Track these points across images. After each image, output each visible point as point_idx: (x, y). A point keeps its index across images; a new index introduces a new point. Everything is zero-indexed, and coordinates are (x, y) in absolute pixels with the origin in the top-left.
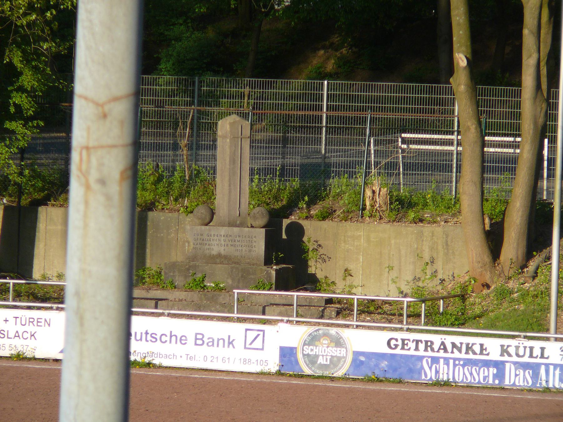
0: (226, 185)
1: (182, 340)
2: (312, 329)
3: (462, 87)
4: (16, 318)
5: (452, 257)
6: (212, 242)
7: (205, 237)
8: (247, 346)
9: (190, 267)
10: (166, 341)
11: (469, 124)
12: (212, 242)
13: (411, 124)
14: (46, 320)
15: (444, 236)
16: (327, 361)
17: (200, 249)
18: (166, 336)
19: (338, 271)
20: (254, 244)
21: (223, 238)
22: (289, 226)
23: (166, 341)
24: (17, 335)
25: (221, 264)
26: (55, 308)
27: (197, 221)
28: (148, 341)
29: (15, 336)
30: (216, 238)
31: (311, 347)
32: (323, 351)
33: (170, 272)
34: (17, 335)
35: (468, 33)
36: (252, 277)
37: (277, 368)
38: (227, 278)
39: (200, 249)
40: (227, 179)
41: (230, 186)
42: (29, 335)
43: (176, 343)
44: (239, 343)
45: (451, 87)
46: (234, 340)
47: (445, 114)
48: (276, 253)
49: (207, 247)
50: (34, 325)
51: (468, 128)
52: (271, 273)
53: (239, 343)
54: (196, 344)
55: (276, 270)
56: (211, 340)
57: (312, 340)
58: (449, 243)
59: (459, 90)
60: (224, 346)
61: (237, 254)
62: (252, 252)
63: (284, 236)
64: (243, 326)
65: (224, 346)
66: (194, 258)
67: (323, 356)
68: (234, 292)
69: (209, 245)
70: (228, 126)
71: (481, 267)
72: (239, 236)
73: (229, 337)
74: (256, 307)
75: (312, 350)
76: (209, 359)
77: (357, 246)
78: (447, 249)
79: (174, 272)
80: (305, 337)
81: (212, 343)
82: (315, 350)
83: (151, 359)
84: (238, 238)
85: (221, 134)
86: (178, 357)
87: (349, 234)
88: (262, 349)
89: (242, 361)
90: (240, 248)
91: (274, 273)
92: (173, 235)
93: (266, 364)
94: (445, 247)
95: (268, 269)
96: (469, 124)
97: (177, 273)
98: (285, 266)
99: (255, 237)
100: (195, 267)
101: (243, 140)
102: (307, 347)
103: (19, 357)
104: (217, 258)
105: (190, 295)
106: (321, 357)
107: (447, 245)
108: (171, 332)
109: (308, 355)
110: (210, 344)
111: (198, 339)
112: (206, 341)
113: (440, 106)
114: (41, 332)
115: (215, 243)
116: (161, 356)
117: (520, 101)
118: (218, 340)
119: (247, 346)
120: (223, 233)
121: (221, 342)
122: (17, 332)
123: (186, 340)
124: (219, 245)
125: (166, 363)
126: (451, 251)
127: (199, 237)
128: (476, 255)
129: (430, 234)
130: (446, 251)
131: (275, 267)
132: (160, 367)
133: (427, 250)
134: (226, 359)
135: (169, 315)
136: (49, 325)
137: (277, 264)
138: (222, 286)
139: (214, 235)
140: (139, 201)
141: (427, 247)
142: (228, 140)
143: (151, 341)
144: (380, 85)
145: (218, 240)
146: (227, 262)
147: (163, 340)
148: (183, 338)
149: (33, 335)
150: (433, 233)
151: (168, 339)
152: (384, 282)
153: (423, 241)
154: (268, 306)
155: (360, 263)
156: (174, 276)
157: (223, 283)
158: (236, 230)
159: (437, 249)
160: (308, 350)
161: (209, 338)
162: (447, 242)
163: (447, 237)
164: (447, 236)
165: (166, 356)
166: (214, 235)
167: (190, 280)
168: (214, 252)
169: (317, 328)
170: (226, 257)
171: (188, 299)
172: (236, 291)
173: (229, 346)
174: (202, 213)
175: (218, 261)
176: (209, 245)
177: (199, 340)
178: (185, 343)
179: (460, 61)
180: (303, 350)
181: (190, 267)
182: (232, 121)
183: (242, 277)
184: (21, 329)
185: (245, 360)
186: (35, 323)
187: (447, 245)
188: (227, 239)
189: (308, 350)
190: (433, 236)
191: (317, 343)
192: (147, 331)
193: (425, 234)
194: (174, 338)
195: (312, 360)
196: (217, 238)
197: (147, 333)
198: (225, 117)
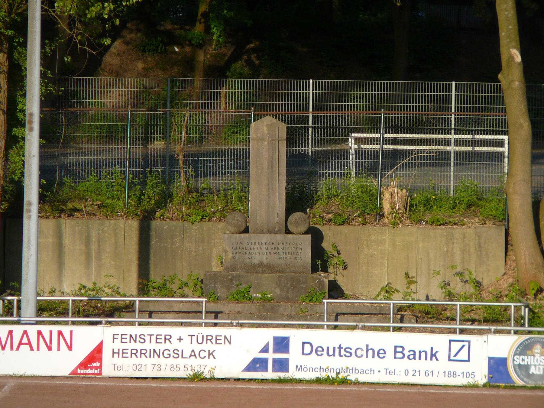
1: (381, 354)
2: (524, 337)
3: (517, 83)
4: (192, 336)
6: (253, 250)
7: (245, 245)
8: (452, 358)
10: (362, 356)
11: (522, 121)
12: (253, 250)
13: (404, 123)
14: (131, 336)
15: (477, 238)
16: (539, 371)
18: (205, 351)
19: (361, 278)
20: (300, 251)
21: (264, 246)
23: (362, 356)
24: (193, 354)
26: (235, 324)
27: (232, 229)
28: (342, 356)
29: (191, 356)
30: (257, 246)
31: (523, 357)
32: (535, 361)
33: (211, 284)
34: (193, 354)
35: (516, 27)
36: (303, 286)
37: (485, 380)
42: (207, 354)
43: (373, 357)
44: (443, 355)
45: (500, 85)
46: (437, 352)
47: (440, 111)
49: (247, 255)
50: (212, 343)
51: (521, 126)
53: (443, 355)
54: (395, 358)
56: (412, 353)
57: (524, 349)
58: (482, 245)
59: (513, 86)
60: (426, 359)
62: (297, 260)
64: (446, 338)
65: (426, 359)
66: (233, 268)
67: (535, 366)
68: (324, 302)
69: (249, 253)
70: (265, 128)
71: (535, 269)
72: (283, 244)
73: (432, 349)
75: (523, 360)
76: (411, 373)
77: (381, 250)
78: (481, 251)
79: (215, 283)
81: (414, 355)
82: (526, 360)
83: (346, 374)
84: (281, 246)
85: (254, 136)
86: (376, 372)
87: (373, 238)
88: (468, 361)
89: (447, 374)
90: (285, 256)
92: (178, 244)
93: (473, 376)
96: (522, 121)
97: (218, 285)
99: (301, 244)
100: (239, 277)
102: (518, 357)
103: (197, 377)
104: (259, 267)
106: (533, 367)
107: (480, 247)
108: (367, 346)
109: (519, 365)
110: (412, 357)
112: (406, 353)
113: (434, 104)
114: (220, 350)
115: (256, 251)
116: (357, 371)
117: (503, 96)
118: (420, 352)
119: (452, 358)
120: (264, 241)
121: (423, 355)
122: (193, 351)
123: (385, 353)
125: (362, 378)
126: (484, 253)
127: (238, 246)
128: (529, 256)
129: (462, 236)
130: (479, 253)
132: (357, 383)
133: (458, 253)
134: (429, 373)
135: (364, 328)
136: (230, 343)
138: (269, 296)
139: (255, 243)
141: (458, 249)
142: (266, 143)
143: (345, 355)
144: (434, 83)
145: (259, 248)
146: (270, 271)
147: (202, 356)
148: (382, 352)
149: (212, 354)
151: (364, 353)
153: (453, 243)
156: (215, 287)
160: (519, 360)
161: (409, 351)
164: (480, 238)
165: (363, 372)
166: (255, 243)
168: (256, 261)
169: (528, 336)
173: (431, 359)
174: (238, 220)
175: (260, 270)
176: (249, 253)
177: (399, 352)
178: (384, 357)
179: (515, 57)
180: (514, 360)
181: (233, 277)
182: (269, 123)
183: (291, 286)
184: (197, 348)
185: (450, 373)
186: (214, 341)
187: (480, 247)
188: (269, 247)
189: (519, 360)
191: (529, 352)
192: (340, 345)
193: (456, 236)
194: (370, 352)
195: (524, 369)
196: (259, 246)
197: (340, 347)
198: (258, 119)
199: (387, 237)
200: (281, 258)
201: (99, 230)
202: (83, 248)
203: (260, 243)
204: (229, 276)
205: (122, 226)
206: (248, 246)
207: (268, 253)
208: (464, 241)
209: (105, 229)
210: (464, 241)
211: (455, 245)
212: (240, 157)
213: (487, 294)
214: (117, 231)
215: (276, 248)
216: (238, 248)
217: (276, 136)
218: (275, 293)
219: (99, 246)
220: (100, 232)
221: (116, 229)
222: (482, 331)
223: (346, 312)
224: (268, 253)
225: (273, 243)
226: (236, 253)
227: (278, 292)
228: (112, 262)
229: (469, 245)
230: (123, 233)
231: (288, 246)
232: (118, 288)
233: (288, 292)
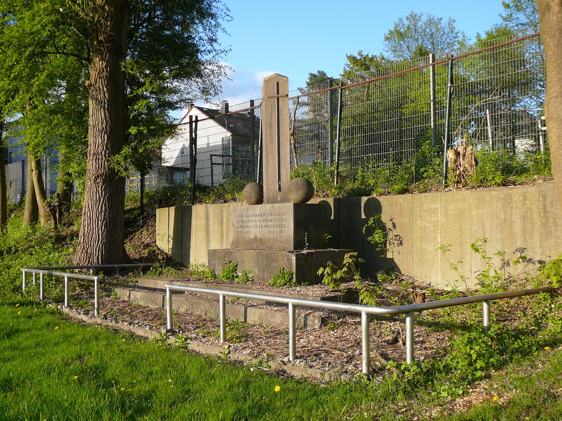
5: (553, 229)
7: (245, 218)
15: (541, 199)
19: (415, 255)
36: (275, 264)
38: (254, 267)
49: (246, 229)
61: (270, 236)
62: (283, 234)
77: (434, 222)
84: (270, 218)
87: (425, 207)
90: (272, 229)
94: (542, 215)
98: (332, 249)
101: (280, 99)
107: (545, 211)
120: (258, 213)
126: (551, 220)
129: (522, 198)
130: (544, 220)
140: (147, 190)
141: (518, 217)
150: (525, 196)
152: (467, 268)
153: (512, 208)
155: (437, 244)
156: (214, 264)
159: (531, 217)
162: (545, 206)
163: (544, 201)
164: (545, 198)
168: (252, 236)
183: (266, 265)
187: (545, 211)
190: (525, 200)
199: (439, 205)
200: (270, 232)
202: (220, 228)
206: (246, 219)
208: (524, 205)
210: (524, 205)
211: (514, 211)
213: (516, 343)
222: (37, 277)
223: (445, 303)
227: (256, 270)
229: (531, 209)
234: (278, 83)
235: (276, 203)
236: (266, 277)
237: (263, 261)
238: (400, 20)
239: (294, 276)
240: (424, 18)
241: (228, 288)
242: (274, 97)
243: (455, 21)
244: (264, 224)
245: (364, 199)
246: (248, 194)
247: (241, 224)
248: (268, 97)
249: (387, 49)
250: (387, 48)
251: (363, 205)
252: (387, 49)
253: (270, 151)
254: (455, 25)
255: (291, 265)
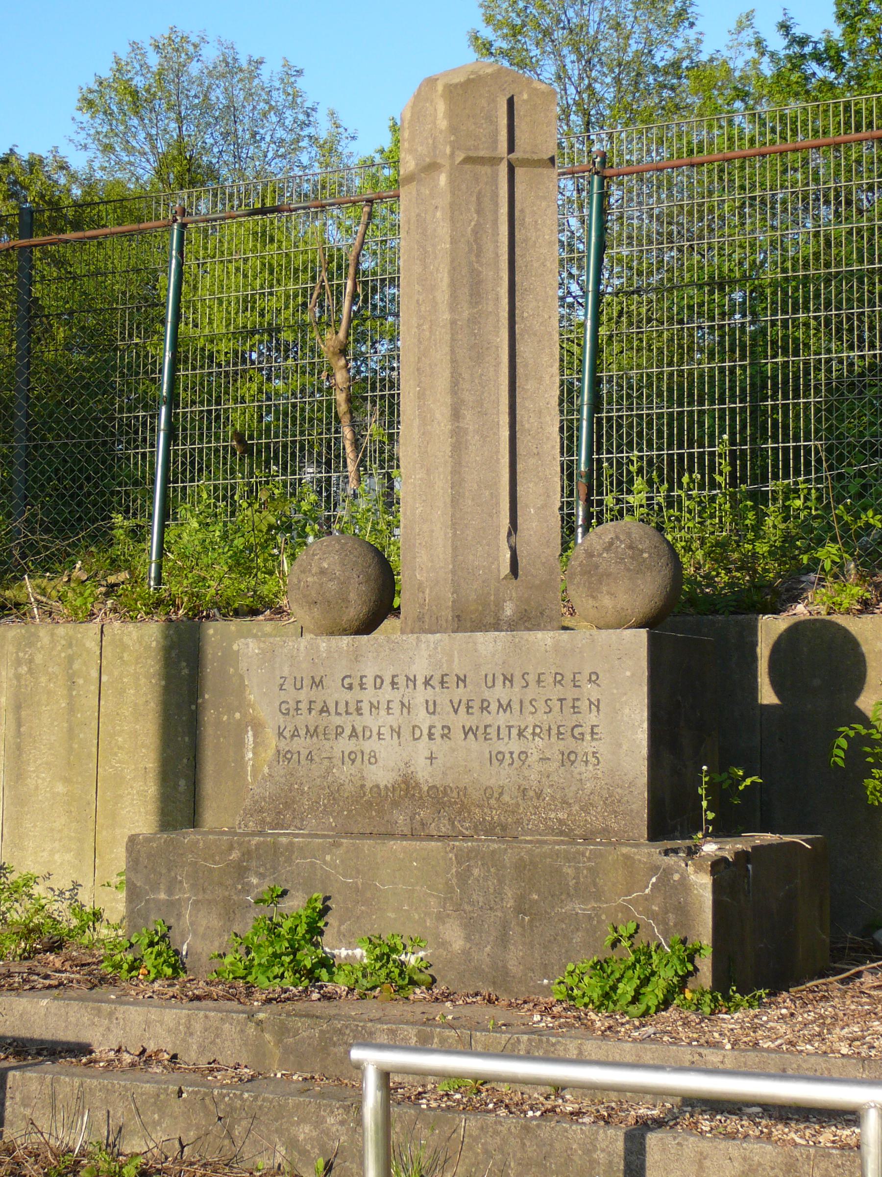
0: (441, 412)
6: (368, 720)
7: (334, 694)
9: (247, 854)
12: (368, 720)
17: (310, 758)
20: (592, 718)
22: (785, 645)
25: (413, 836)
30: (387, 693)
33: (155, 888)
36: (578, 907)
38: (441, 918)
39: (310, 758)
40: (443, 381)
41: (456, 415)
48: (722, 766)
49: (345, 745)
52: (684, 885)
55: (718, 866)
61: (501, 777)
63: (767, 696)
68: (359, 1067)
70: (441, 107)
72: (508, 679)
74: (577, 1132)
80: (702, 47)
84: (500, 692)
90: (515, 746)
91: (702, 884)
95: (671, 860)
97: (185, 893)
98: (769, 838)
99: (594, 678)
101: (519, 172)
104: (395, 804)
105: (198, 1027)
111: (580, 1053)
120: (420, 668)
124: (406, 733)
127: (303, 695)
131: (710, 848)
137: (724, 828)
138: (412, 960)
145: (396, 706)
154: (659, 1123)
156: (171, 904)
157: (417, 943)
158: (488, 644)
167: (248, 925)
168: (381, 775)
170: (440, 798)
171: (191, 1056)
172: (370, 1059)
174: (323, 572)
175: (401, 819)
176: (354, 734)
181: (247, 854)
183: (519, 910)
188: (443, 698)
200: (499, 757)
201: (18, 662)
203: (401, 680)
204: (231, 848)
205: (92, 645)
206: (348, 696)
207: (437, 732)
209: (39, 659)
212: (701, 403)
214: (76, 666)
215: (476, 705)
216: (304, 706)
217: (495, 142)
218: (444, 945)
219: (19, 724)
220: (24, 669)
221: (70, 660)
224: (437, 732)
225: (461, 680)
226: (295, 734)
227: (455, 937)
228: (60, 788)
230: (95, 674)
231: (532, 692)
232: (76, 886)
233: (503, 940)
234: (511, 102)
235: (496, 627)
236: (513, 966)
237: (499, 893)
238: (135, 46)
239: (705, 964)
240: (210, 54)
241: (411, 1033)
242: (494, 161)
243: (300, 73)
244: (462, 719)
245: (770, 628)
246: (332, 586)
247: (312, 719)
248: (468, 160)
249: (81, 138)
250: (83, 134)
251: (763, 651)
252: (81, 138)
253: (467, 397)
254: (301, 84)
255: (684, 912)
